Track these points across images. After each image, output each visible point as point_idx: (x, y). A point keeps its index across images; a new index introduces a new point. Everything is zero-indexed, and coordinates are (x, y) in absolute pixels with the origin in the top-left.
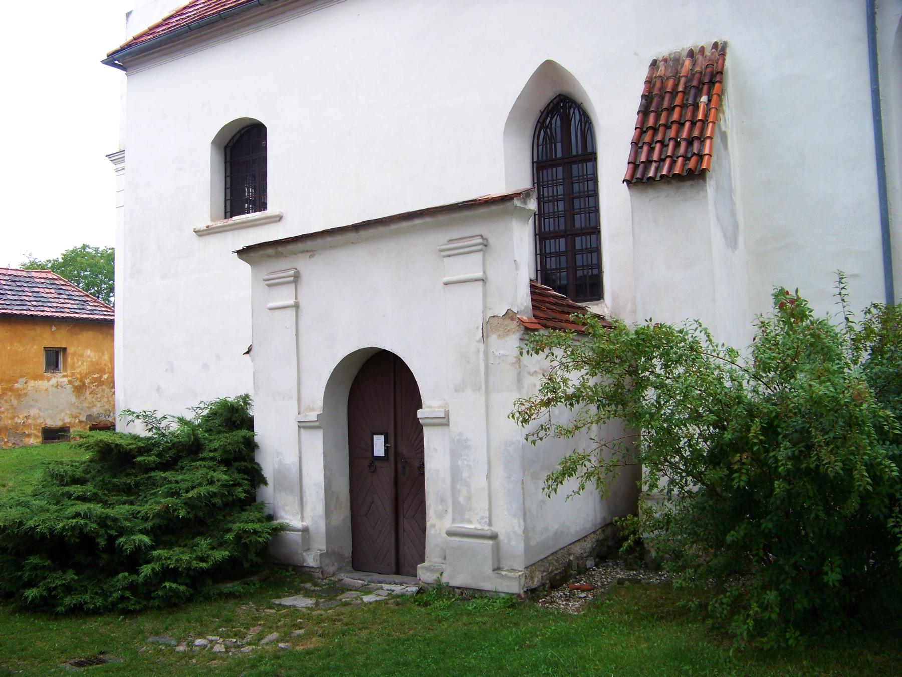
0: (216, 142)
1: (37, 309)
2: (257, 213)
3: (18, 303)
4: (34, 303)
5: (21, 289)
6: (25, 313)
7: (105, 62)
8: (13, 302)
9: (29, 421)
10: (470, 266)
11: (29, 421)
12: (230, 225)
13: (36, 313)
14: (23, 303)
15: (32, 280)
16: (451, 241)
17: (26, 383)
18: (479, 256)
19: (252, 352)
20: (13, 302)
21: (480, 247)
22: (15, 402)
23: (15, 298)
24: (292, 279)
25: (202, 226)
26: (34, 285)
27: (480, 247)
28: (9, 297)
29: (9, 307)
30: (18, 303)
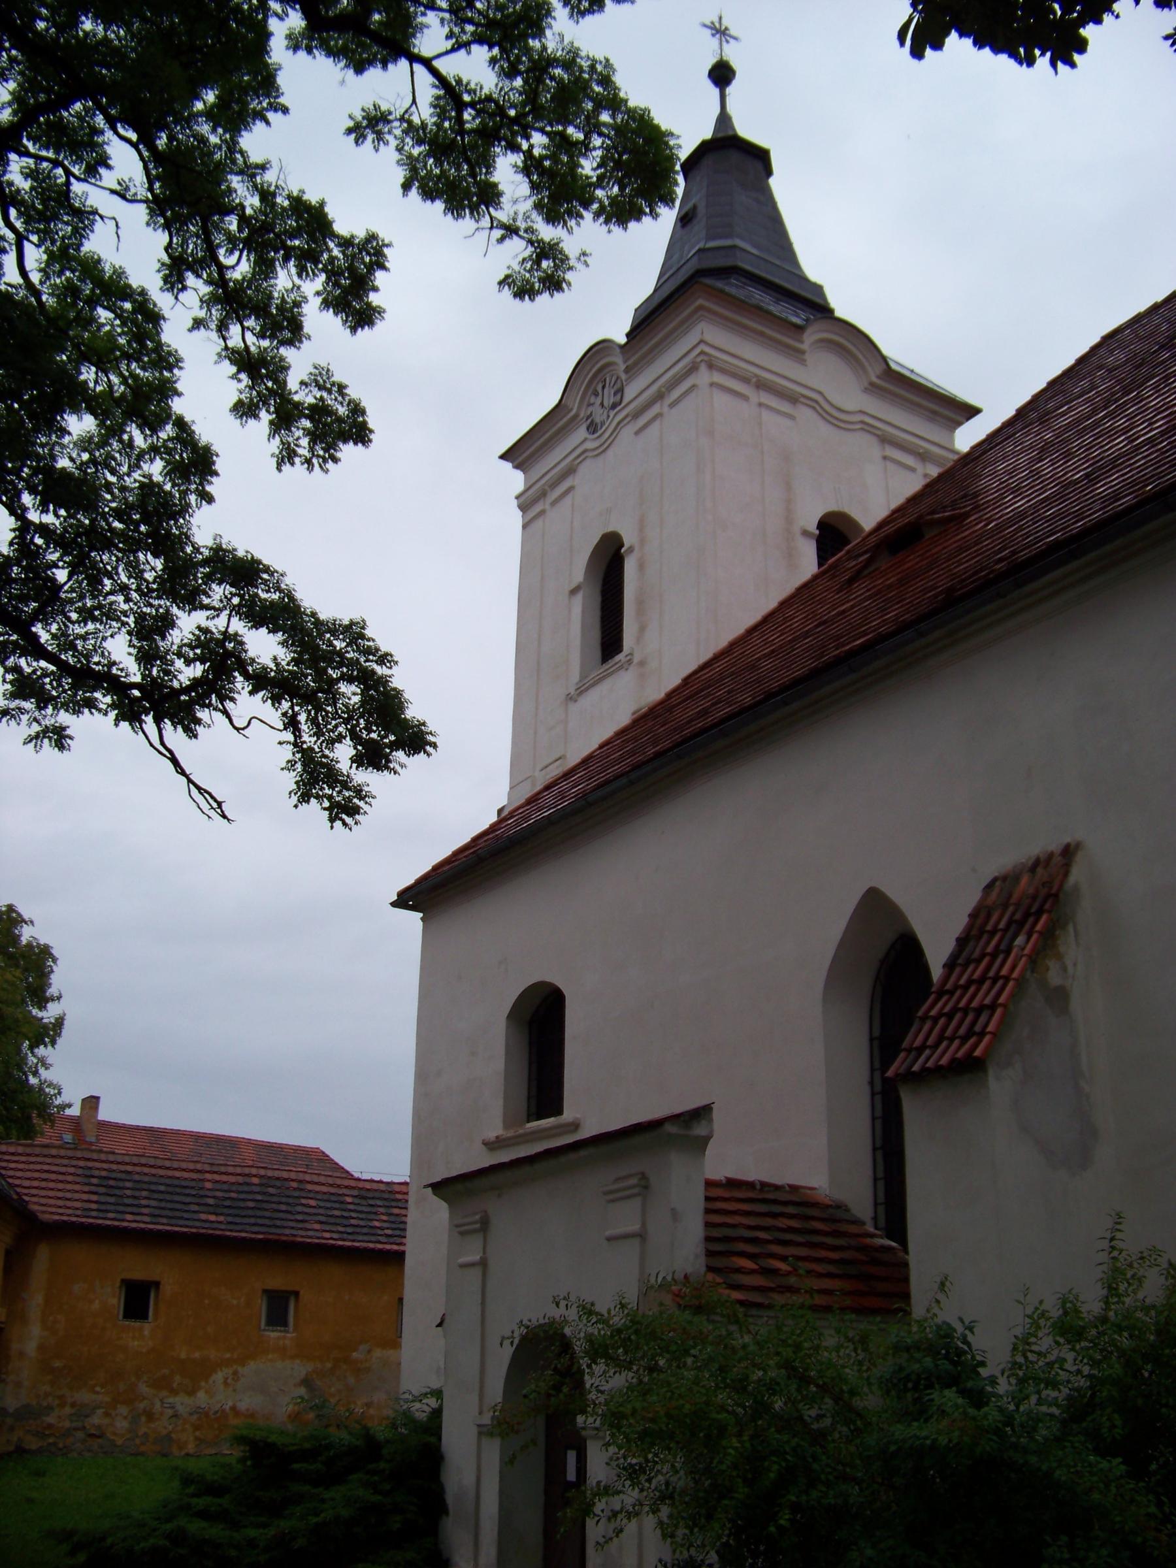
0: (515, 1014)
1: (392, 1240)
2: (552, 1120)
3: (365, 1230)
4: (389, 1232)
5: (374, 1210)
6: (371, 1245)
7: (394, 904)
8: (358, 1230)
9: (372, 1411)
10: (626, 1218)
11: (372, 1411)
12: (520, 1136)
13: (388, 1247)
14: (373, 1231)
15: (392, 1196)
16: (618, 1180)
17: (369, 1351)
18: (637, 1203)
19: (445, 1325)
20: (358, 1230)
21: (635, 1191)
22: (351, 1380)
23: (362, 1223)
24: (478, 1226)
25: (491, 1135)
26: (394, 1204)
27: (635, 1191)
28: (353, 1222)
29: (350, 1237)
30: (365, 1230)
